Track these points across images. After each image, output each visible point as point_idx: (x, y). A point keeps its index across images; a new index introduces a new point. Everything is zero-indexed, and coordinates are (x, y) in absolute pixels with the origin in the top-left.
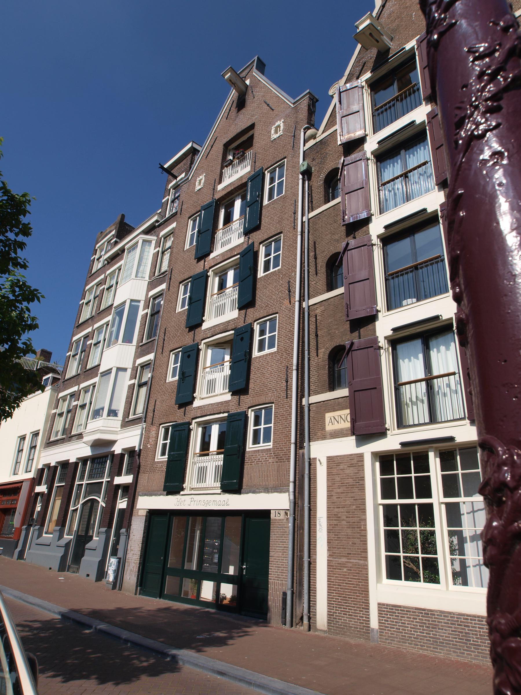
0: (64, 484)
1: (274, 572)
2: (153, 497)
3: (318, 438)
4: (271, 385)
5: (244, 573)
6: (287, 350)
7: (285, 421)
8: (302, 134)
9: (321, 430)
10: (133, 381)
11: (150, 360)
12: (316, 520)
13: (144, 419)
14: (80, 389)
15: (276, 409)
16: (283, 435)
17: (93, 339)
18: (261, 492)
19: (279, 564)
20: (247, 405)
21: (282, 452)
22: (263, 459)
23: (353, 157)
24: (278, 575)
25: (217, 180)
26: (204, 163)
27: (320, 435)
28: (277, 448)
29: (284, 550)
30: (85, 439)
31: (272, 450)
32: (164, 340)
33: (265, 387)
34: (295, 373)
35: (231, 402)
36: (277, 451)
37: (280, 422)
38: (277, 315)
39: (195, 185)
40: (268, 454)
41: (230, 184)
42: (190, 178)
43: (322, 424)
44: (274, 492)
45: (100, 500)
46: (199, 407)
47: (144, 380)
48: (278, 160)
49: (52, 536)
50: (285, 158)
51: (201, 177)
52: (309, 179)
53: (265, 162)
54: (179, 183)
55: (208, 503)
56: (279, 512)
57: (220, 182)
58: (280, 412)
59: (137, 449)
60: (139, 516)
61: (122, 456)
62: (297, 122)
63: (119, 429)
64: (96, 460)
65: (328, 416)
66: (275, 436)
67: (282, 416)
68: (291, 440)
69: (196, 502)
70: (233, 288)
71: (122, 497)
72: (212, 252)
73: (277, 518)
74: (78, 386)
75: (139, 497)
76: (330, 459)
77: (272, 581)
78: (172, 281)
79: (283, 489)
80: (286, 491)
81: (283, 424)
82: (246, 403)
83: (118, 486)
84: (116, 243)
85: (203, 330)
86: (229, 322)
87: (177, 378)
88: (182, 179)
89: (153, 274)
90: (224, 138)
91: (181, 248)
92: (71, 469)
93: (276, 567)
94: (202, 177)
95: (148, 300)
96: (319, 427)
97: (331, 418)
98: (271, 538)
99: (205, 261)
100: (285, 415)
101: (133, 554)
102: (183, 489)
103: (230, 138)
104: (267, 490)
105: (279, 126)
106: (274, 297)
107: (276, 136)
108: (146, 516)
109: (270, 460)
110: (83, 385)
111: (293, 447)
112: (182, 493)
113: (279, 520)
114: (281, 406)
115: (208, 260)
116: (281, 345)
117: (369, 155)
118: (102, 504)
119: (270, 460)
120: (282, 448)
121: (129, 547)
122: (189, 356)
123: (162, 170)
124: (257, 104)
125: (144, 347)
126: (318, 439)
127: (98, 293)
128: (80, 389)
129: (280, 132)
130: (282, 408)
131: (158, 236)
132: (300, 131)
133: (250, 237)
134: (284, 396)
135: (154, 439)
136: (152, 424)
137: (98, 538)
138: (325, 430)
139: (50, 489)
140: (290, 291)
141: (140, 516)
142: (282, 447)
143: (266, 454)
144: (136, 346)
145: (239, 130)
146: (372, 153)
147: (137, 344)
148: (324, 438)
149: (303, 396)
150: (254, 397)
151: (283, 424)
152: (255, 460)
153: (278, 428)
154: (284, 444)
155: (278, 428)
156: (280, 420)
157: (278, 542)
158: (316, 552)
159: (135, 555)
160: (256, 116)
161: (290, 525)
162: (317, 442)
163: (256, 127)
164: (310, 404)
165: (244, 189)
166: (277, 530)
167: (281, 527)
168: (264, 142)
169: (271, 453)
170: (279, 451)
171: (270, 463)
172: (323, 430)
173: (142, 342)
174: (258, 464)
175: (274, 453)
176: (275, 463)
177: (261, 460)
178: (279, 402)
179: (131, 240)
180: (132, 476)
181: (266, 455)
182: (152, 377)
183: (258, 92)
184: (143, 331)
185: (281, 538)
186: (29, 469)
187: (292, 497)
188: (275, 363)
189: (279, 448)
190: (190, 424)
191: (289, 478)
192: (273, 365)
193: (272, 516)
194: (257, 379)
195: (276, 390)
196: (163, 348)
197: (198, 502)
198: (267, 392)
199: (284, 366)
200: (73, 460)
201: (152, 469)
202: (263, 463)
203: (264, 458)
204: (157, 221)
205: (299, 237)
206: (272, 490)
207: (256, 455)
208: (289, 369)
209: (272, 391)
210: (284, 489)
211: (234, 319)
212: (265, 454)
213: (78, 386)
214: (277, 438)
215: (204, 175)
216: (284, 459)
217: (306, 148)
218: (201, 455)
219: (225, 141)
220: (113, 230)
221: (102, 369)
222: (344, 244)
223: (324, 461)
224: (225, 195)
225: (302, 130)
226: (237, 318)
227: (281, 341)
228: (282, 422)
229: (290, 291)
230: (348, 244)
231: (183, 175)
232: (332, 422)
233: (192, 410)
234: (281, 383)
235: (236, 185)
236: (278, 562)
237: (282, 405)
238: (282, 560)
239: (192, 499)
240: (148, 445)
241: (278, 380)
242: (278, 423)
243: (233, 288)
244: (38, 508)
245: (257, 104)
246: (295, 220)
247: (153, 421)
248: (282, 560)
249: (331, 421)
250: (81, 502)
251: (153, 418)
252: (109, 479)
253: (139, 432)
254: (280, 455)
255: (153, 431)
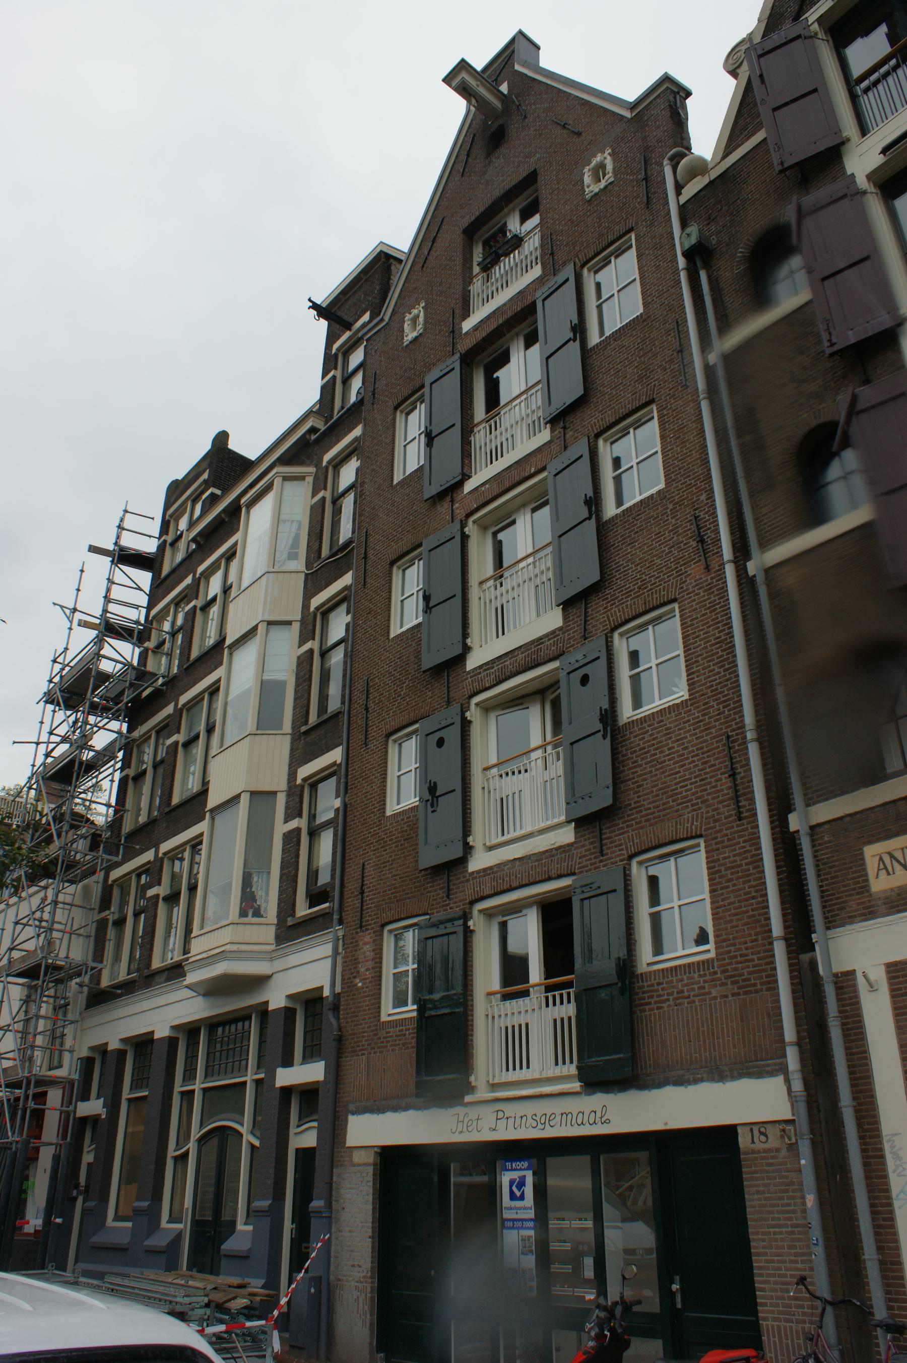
0: (146, 1093)
1: (771, 1297)
2: (390, 1115)
3: (849, 917)
4: (686, 791)
5: (679, 1306)
6: (720, 693)
7: (744, 882)
8: (668, 170)
9: (858, 894)
10: (294, 824)
11: (334, 764)
12: (881, 1143)
13: (336, 917)
14: (160, 855)
15: (713, 851)
16: (742, 919)
17: (179, 732)
18: (702, 1080)
19: (785, 1276)
20: (624, 852)
21: (748, 967)
22: (693, 990)
23: (821, 193)
24: (784, 1306)
25: (457, 311)
26: (418, 280)
27: (855, 907)
28: (730, 958)
29: (792, 1233)
30: (192, 977)
31: (716, 964)
32: (367, 709)
33: (671, 796)
34: (753, 752)
35: (576, 848)
36: (731, 964)
37: (728, 887)
38: (676, 605)
39: (403, 331)
40: (705, 975)
41: (494, 312)
42: (387, 318)
43: (859, 877)
44: (741, 1076)
45: (244, 1130)
46: (485, 870)
47: (322, 818)
48: (611, 238)
49: (129, 1224)
50: (630, 230)
51: (415, 312)
52: (707, 266)
53: (577, 248)
54: (360, 335)
55: (548, 1120)
56: (763, 1130)
57: (466, 314)
58: (724, 858)
59: (326, 993)
60: (354, 1165)
61: (289, 1013)
62: (646, 148)
63: (273, 947)
64: (220, 1030)
65: (872, 852)
66: (719, 924)
67: (733, 867)
68: (770, 931)
69: (511, 1121)
70: (496, 580)
71: (303, 1117)
72: (470, 477)
73: (759, 1146)
74: (153, 850)
75: (351, 1118)
76: (897, 971)
77: (770, 1323)
78: (369, 562)
79: (764, 1066)
80: (778, 1071)
81: (739, 890)
82: (621, 845)
83: (287, 1091)
84: (214, 499)
85: (469, 672)
86: (539, 641)
87: (418, 799)
88: (364, 325)
89: (317, 555)
90: (463, 217)
91: (385, 480)
92: (159, 1057)
93: (775, 1283)
94: (419, 311)
95: (311, 618)
96: (848, 885)
97: (881, 859)
98: (747, 1203)
99: (452, 501)
100: (741, 865)
101: (353, 1266)
102: (471, 1089)
103: (477, 214)
104: (718, 1074)
105: (602, 166)
106: (659, 561)
107: (596, 188)
108: (375, 1165)
109: (713, 991)
110: (165, 847)
111: (779, 950)
112: (468, 1099)
113: (765, 1151)
114: (726, 843)
115: (459, 498)
116: (699, 681)
117: (862, 182)
118: (249, 1139)
119: (713, 991)
120: (746, 955)
121: (332, 1254)
122: (440, 743)
123: (315, 313)
124: (536, 130)
125: (314, 735)
126: (851, 919)
127: (180, 621)
128: (160, 855)
129: (607, 177)
130: (727, 847)
131: (318, 465)
132: (661, 165)
133: (567, 426)
134: (731, 816)
135: (370, 964)
136: (361, 927)
137: (250, 1228)
138: (868, 891)
139: (113, 1107)
140: (702, 541)
141: (359, 1165)
142: (745, 952)
143: (700, 976)
144: (293, 734)
145: (497, 194)
146: (869, 177)
147: (293, 728)
148: (869, 913)
149: (788, 808)
150: (641, 828)
151: (739, 890)
152: (668, 994)
153: (726, 902)
154: (749, 944)
155: (726, 902)
156: (727, 881)
157: (772, 1212)
158: (895, 1234)
159: (357, 1268)
160: (538, 155)
161: (803, 1162)
162: (849, 927)
163: (541, 178)
164: (812, 828)
165: (530, 320)
166: (763, 1179)
167: (773, 1171)
168: (567, 207)
169: (716, 973)
170: (737, 963)
171: (715, 998)
172: (862, 893)
173: (306, 722)
174: (680, 1004)
175: (723, 972)
176: (730, 998)
177: (686, 994)
178: (717, 832)
179: (251, 486)
180: (323, 1063)
181: (702, 980)
182: (345, 806)
183: (534, 104)
184: (306, 695)
185: (780, 1202)
186: (56, 1063)
187: (798, 1085)
188: (689, 731)
189: (735, 957)
190: (466, 916)
191: (782, 1035)
192: (686, 737)
193: (744, 1140)
194: (645, 780)
195: (702, 802)
196: (367, 731)
197: (518, 1120)
198: (677, 811)
199: (717, 736)
200: (162, 1032)
201: (376, 1043)
202: (694, 1002)
203: (696, 986)
204: (313, 430)
205: (705, 406)
206: (731, 1070)
207: (672, 982)
208: (733, 742)
209: (692, 805)
210: (768, 1065)
211: (553, 632)
212: (696, 976)
213: (153, 850)
214: (726, 929)
215: (423, 305)
216: (755, 985)
217: (683, 199)
218: (506, 997)
219: (464, 223)
220: (204, 471)
221: (212, 802)
222: (844, 399)
223: (879, 975)
224: (484, 339)
225: (666, 162)
226: (560, 629)
227: (698, 671)
228: (734, 885)
229: (702, 541)
230: (854, 398)
231: (366, 317)
232: (886, 868)
233: (468, 880)
234: (717, 781)
235: (510, 314)
236: (780, 1269)
237: (729, 840)
238: (791, 1262)
239: (500, 1115)
240: (357, 980)
241: (706, 773)
242: (722, 889)
243: (496, 580)
244: (88, 1157)
245: (536, 130)
246: (686, 365)
247: (361, 918)
248: (791, 1262)
249: (882, 866)
250: (195, 1133)
251: (362, 910)
252: (262, 1076)
253: (327, 949)
254: (743, 975)
255: (365, 944)
